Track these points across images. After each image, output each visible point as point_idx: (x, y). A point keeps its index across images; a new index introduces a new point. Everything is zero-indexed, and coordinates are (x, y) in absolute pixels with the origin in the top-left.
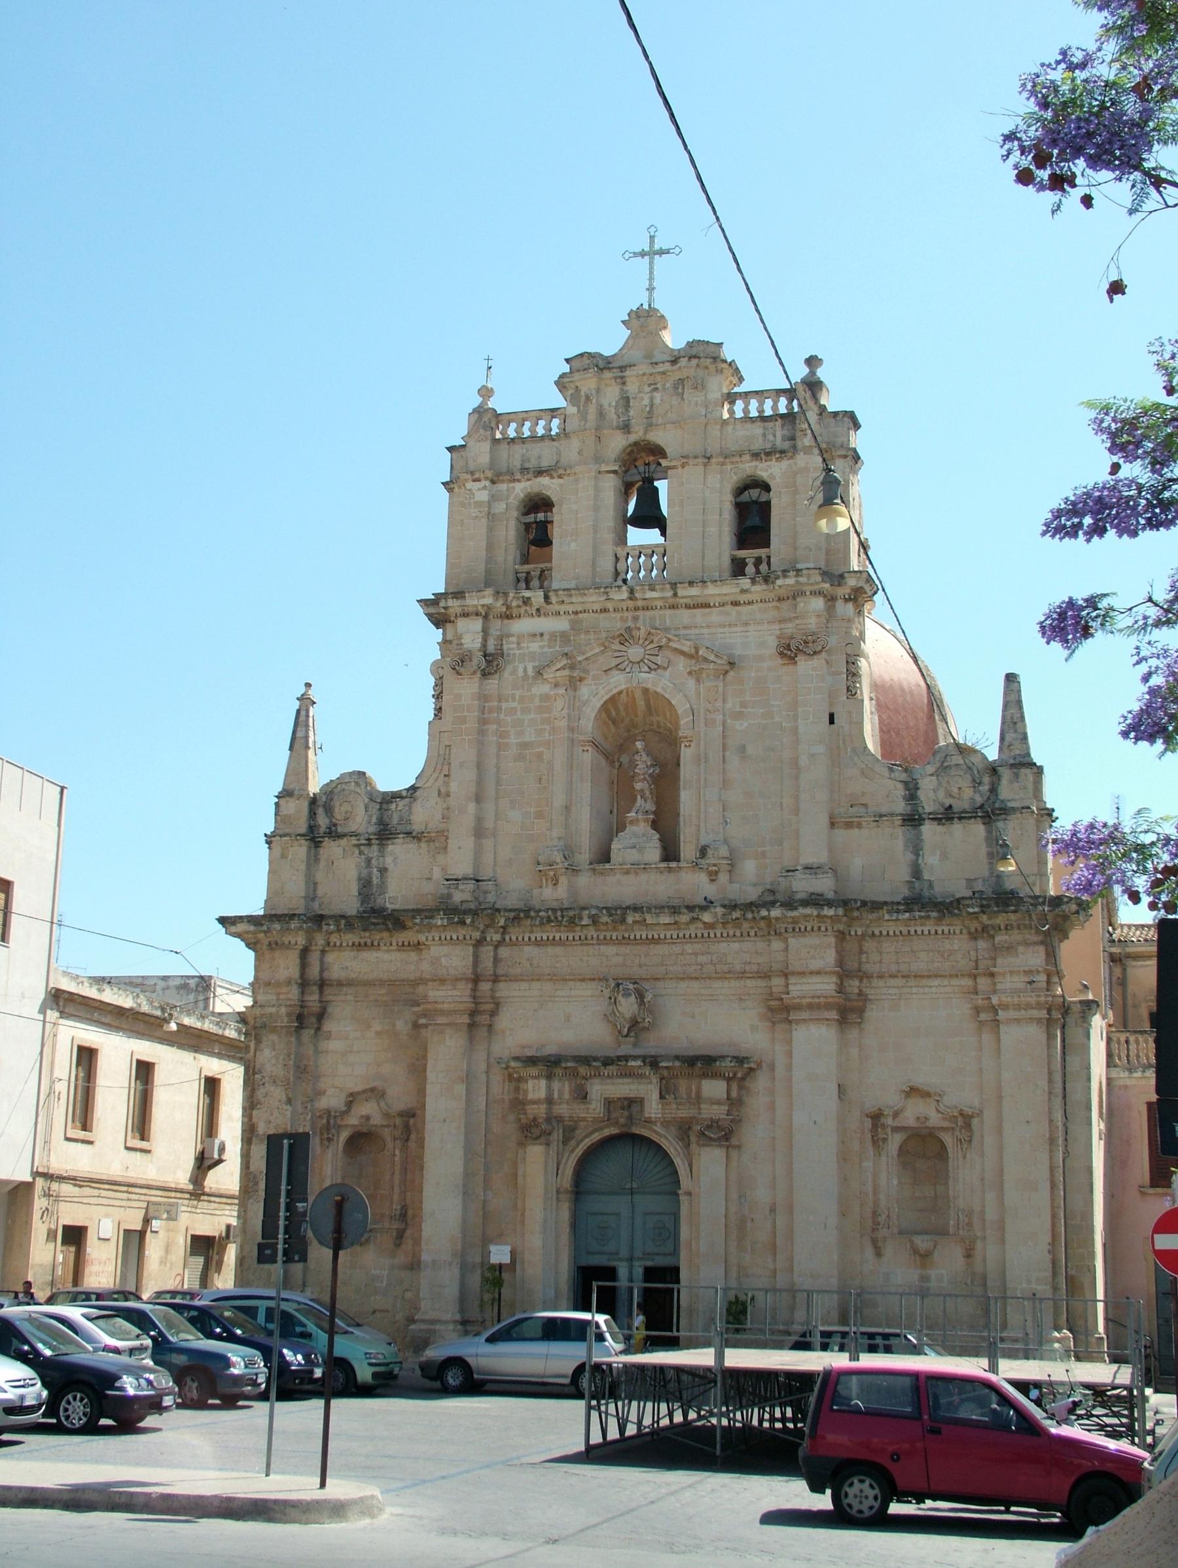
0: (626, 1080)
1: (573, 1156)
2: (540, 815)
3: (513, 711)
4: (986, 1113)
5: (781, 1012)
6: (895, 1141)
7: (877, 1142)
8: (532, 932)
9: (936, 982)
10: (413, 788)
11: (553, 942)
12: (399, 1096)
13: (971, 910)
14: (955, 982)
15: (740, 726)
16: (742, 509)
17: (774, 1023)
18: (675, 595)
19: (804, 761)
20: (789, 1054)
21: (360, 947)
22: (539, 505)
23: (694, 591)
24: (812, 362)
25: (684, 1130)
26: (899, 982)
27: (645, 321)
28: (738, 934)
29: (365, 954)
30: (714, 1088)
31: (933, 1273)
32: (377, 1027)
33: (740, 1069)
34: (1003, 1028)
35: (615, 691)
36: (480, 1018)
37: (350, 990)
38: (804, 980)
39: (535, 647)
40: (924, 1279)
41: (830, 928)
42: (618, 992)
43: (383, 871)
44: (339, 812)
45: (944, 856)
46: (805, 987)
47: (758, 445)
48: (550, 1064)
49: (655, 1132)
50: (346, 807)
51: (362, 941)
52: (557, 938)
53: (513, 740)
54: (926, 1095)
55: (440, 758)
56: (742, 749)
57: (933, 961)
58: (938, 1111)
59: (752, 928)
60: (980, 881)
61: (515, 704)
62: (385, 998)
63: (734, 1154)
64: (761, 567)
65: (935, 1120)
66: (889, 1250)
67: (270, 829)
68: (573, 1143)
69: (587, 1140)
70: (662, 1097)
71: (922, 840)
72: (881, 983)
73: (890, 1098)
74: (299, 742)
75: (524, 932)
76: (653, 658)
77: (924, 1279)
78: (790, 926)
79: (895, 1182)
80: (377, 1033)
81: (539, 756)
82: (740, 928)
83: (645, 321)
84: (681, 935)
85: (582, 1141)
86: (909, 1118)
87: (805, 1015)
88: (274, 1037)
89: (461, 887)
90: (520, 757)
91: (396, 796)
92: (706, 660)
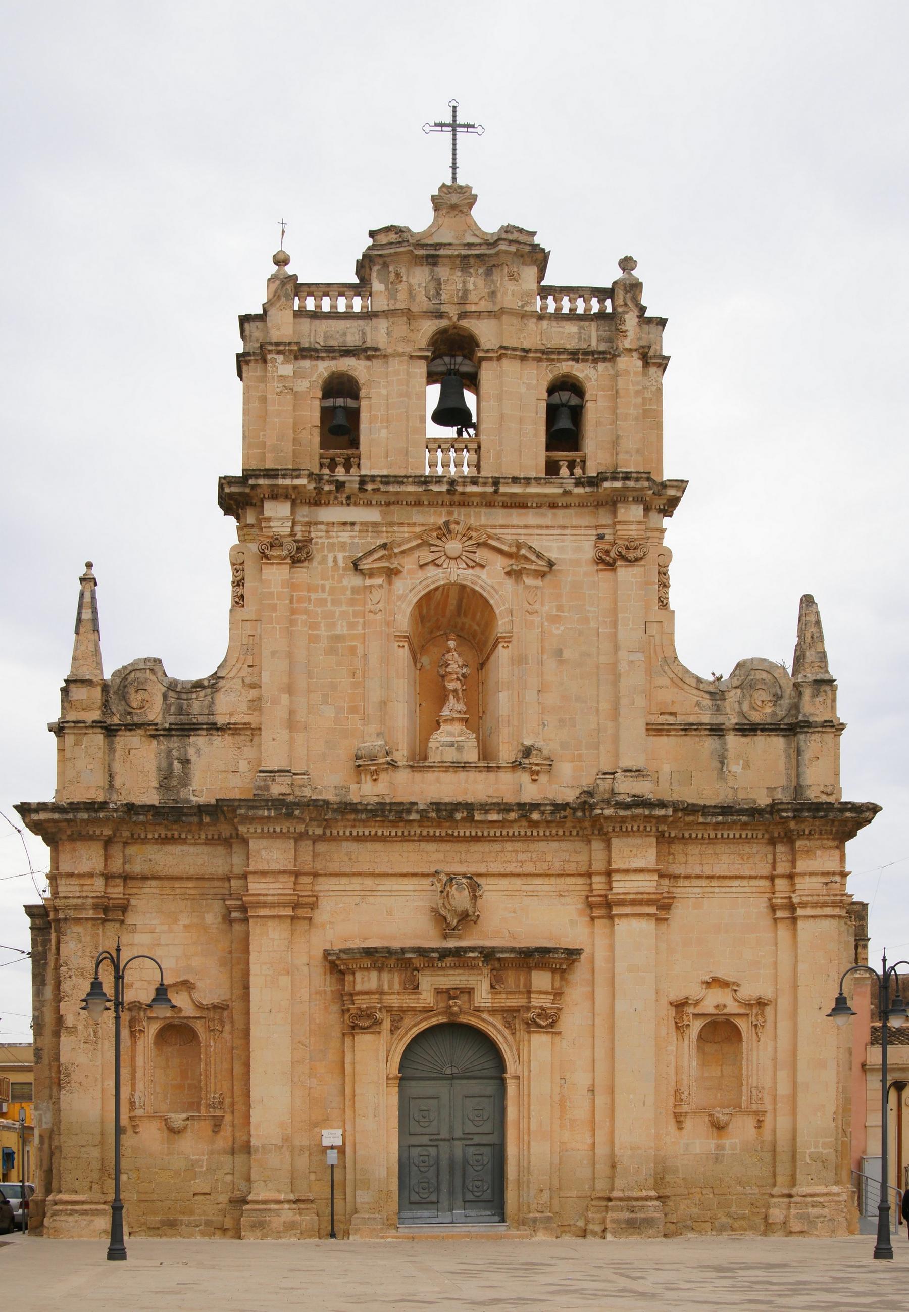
0: (457, 972)
1: (401, 1044)
2: (354, 710)
3: (322, 602)
4: (780, 1001)
5: (603, 908)
6: (697, 1026)
7: (680, 1028)
8: (354, 827)
9: (737, 882)
10: (216, 677)
11: (375, 838)
12: (212, 987)
13: (784, 814)
14: (754, 882)
15: (558, 630)
16: (552, 412)
17: (593, 919)
18: (496, 492)
19: (623, 667)
20: (611, 948)
21: (165, 840)
22: (341, 389)
23: (516, 489)
24: (627, 264)
25: (509, 1015)
26: (704, 882)
27: (453, 201)
28: (560, 833)
29: (170, 848)
30: (541, 980)
31: (727, 1142)
32: (184, 920)
33: (558, 960)
34: (800, 924)
35: (432, 587)
36: (301, 911)
37: (154, 883)
38: (627, 878)
39: (345, 536)
40: (720, 1147)
41: (654, 829)
42: (451, 887)
43: (185, 762)
44: (135, 699)
45: (747, 766)
46: (628, 884)
47: (571, 345)
48: (377, 957)
49: (483, 1020)
50: (141, 695)
51: (169, 834)
52: (380, 833)
53: (323, 632)
54: (725, 984)
55: (246, 646)
56: (559, 653)
57: (734, 863)
58: (736, 1000)
59: (574, 827)
60: (779, 789)
61: (325, 596)
62: (192, 892)
63: (557, 1039)
64: (575, 471)
65: (733, 1008)
66: (688, 1123)
67: (55, 715)
68: (401, 1031)
69: (415, 1029)
70: (492, 987)
71: (726, 750)
72: (687, 883)
73: (694, 990)
74: (87, 621)
75: (346, 827)
76: (471, 555)
77: (720, 1147)
78: (618, 825)
79: (694, 1064)
80: (185, 926)
81: (353, 649)
82: (562, 827)
83: (453, 201)
84: (504, 833)
85: (410, 1029)
86: (708, 1007)
87: (627, 910)
88: (78, 929)
89: (278, 779)
90: (331, 651)
91: (198, 685)
92: (526, 558)
